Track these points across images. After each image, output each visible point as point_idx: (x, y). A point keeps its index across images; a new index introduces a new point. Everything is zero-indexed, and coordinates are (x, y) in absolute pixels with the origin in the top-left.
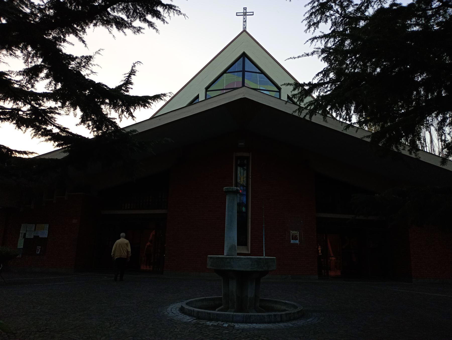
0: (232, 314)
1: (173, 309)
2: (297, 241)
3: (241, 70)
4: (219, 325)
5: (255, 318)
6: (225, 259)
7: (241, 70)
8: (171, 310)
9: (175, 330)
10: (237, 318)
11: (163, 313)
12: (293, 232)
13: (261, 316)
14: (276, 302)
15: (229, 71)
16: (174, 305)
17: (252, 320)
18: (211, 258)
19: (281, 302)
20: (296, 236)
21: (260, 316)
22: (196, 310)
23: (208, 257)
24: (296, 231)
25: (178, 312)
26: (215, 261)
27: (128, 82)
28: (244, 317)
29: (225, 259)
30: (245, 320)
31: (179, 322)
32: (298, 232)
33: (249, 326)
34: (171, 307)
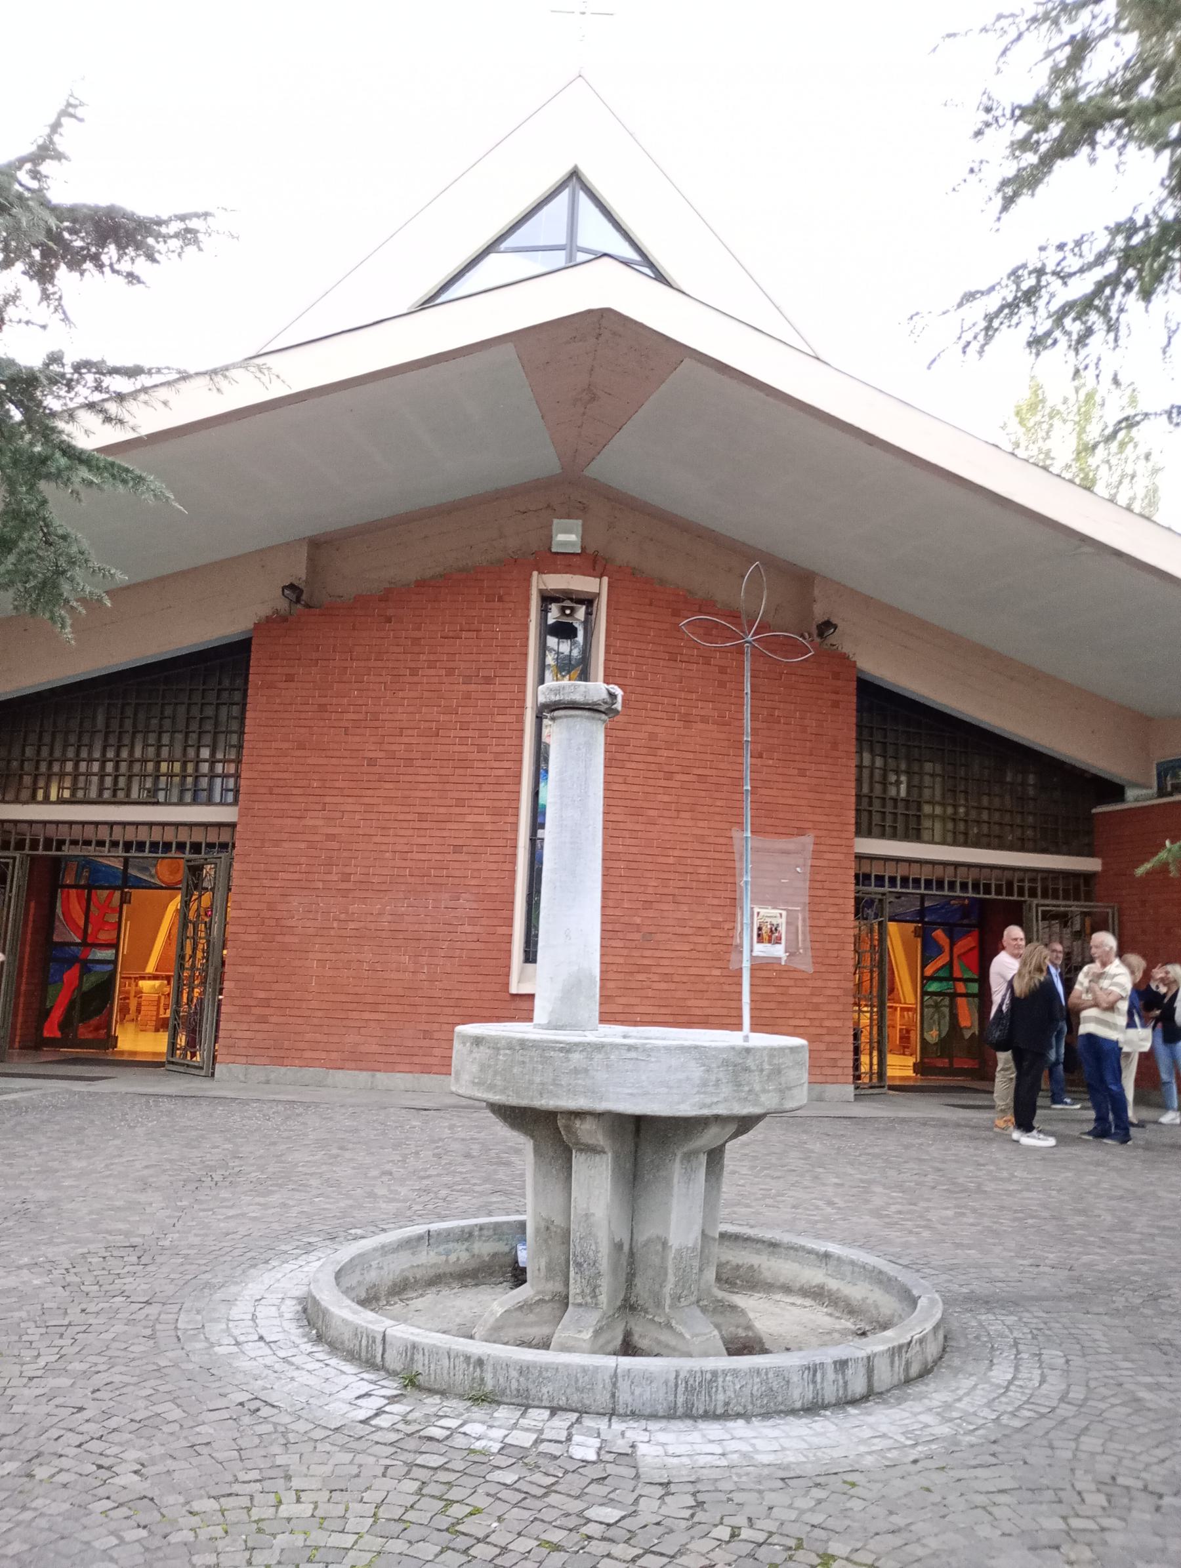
0: (606, 1368)
1: (262, 1312)
2: (777, 946)
3: (562, 240)
4: (543, 1447)
5: (738, 1387)
6: (561, 1050)
7: (562, 240)
8: (254, 1318)
9: (284, 1511)
10: (637, 1391)
11: (212, 1345)
12: (763, 912)
13: (771, 1375)
14: (773, 1246)
15: (503, 246)
16: (268, 1278)
17: (721, 1397)
18: (478, 1041)
19: (803, 1248)
20: (774, 929)
21: (767, 1374)
22: (401, 1338)
23: (465, 1038)
24: (774, 908)
25: (291, 1327)
26: (501, 1057)
27: (46, 152)
28: (676, 1386)
29: (561, 1050)
30: (681, 1400)
31: (302, 1426)
32: (784, 913)
33: (718, 1450)
34: (253, 1289)
